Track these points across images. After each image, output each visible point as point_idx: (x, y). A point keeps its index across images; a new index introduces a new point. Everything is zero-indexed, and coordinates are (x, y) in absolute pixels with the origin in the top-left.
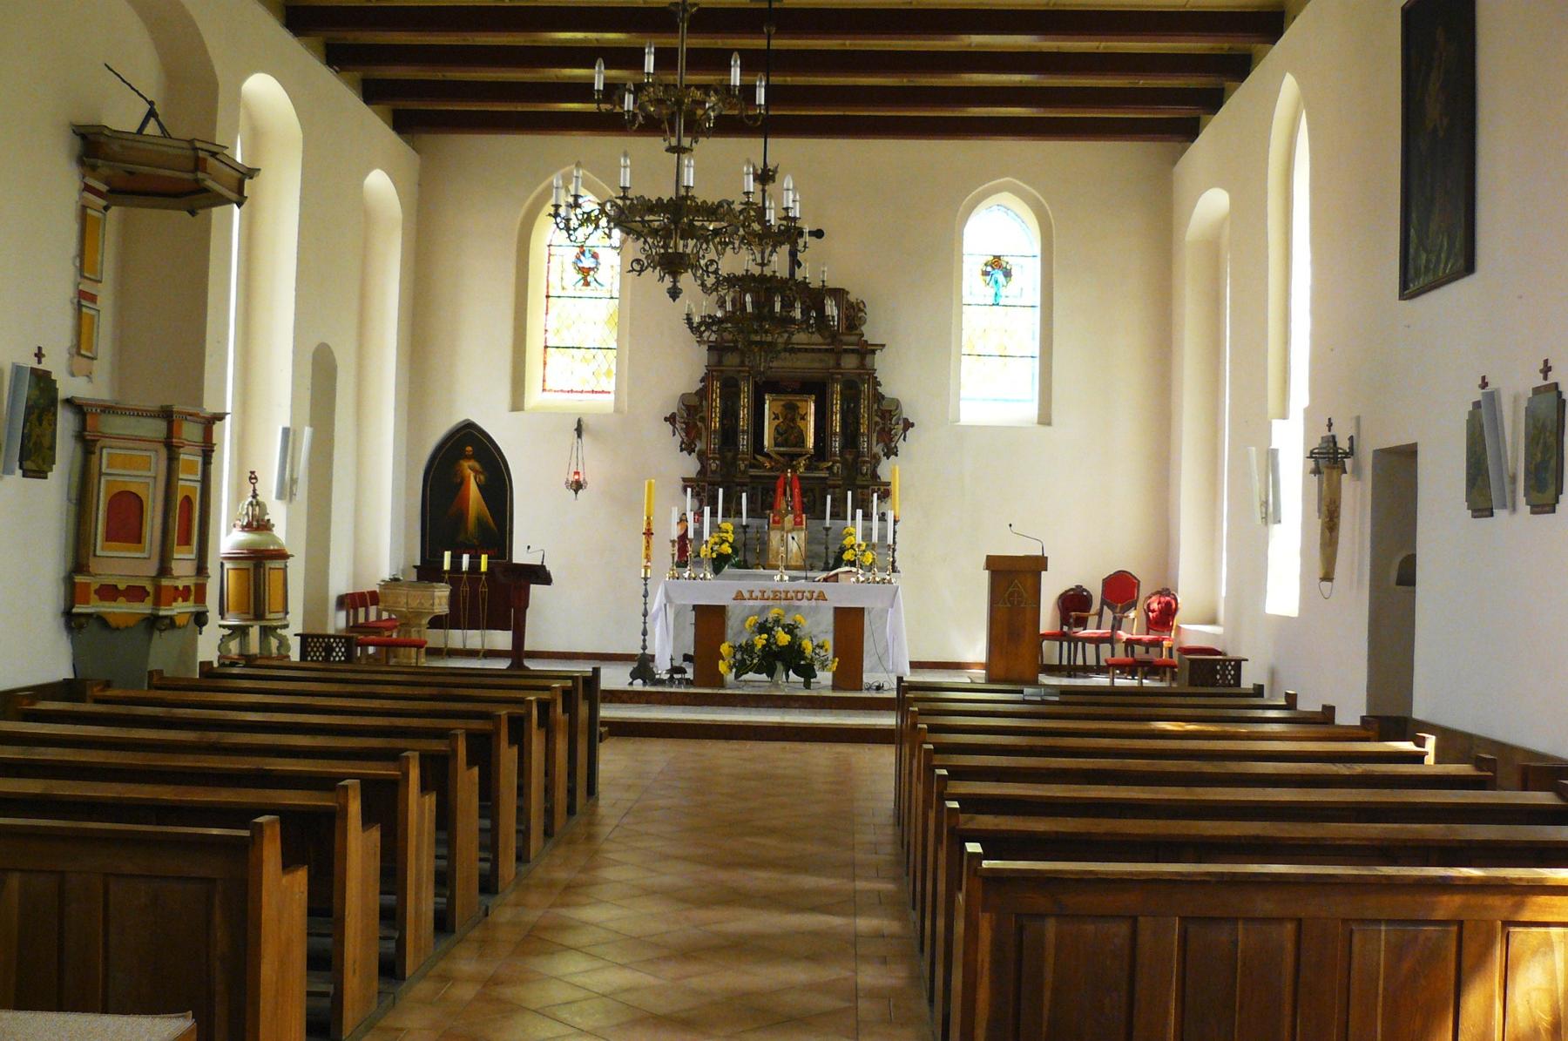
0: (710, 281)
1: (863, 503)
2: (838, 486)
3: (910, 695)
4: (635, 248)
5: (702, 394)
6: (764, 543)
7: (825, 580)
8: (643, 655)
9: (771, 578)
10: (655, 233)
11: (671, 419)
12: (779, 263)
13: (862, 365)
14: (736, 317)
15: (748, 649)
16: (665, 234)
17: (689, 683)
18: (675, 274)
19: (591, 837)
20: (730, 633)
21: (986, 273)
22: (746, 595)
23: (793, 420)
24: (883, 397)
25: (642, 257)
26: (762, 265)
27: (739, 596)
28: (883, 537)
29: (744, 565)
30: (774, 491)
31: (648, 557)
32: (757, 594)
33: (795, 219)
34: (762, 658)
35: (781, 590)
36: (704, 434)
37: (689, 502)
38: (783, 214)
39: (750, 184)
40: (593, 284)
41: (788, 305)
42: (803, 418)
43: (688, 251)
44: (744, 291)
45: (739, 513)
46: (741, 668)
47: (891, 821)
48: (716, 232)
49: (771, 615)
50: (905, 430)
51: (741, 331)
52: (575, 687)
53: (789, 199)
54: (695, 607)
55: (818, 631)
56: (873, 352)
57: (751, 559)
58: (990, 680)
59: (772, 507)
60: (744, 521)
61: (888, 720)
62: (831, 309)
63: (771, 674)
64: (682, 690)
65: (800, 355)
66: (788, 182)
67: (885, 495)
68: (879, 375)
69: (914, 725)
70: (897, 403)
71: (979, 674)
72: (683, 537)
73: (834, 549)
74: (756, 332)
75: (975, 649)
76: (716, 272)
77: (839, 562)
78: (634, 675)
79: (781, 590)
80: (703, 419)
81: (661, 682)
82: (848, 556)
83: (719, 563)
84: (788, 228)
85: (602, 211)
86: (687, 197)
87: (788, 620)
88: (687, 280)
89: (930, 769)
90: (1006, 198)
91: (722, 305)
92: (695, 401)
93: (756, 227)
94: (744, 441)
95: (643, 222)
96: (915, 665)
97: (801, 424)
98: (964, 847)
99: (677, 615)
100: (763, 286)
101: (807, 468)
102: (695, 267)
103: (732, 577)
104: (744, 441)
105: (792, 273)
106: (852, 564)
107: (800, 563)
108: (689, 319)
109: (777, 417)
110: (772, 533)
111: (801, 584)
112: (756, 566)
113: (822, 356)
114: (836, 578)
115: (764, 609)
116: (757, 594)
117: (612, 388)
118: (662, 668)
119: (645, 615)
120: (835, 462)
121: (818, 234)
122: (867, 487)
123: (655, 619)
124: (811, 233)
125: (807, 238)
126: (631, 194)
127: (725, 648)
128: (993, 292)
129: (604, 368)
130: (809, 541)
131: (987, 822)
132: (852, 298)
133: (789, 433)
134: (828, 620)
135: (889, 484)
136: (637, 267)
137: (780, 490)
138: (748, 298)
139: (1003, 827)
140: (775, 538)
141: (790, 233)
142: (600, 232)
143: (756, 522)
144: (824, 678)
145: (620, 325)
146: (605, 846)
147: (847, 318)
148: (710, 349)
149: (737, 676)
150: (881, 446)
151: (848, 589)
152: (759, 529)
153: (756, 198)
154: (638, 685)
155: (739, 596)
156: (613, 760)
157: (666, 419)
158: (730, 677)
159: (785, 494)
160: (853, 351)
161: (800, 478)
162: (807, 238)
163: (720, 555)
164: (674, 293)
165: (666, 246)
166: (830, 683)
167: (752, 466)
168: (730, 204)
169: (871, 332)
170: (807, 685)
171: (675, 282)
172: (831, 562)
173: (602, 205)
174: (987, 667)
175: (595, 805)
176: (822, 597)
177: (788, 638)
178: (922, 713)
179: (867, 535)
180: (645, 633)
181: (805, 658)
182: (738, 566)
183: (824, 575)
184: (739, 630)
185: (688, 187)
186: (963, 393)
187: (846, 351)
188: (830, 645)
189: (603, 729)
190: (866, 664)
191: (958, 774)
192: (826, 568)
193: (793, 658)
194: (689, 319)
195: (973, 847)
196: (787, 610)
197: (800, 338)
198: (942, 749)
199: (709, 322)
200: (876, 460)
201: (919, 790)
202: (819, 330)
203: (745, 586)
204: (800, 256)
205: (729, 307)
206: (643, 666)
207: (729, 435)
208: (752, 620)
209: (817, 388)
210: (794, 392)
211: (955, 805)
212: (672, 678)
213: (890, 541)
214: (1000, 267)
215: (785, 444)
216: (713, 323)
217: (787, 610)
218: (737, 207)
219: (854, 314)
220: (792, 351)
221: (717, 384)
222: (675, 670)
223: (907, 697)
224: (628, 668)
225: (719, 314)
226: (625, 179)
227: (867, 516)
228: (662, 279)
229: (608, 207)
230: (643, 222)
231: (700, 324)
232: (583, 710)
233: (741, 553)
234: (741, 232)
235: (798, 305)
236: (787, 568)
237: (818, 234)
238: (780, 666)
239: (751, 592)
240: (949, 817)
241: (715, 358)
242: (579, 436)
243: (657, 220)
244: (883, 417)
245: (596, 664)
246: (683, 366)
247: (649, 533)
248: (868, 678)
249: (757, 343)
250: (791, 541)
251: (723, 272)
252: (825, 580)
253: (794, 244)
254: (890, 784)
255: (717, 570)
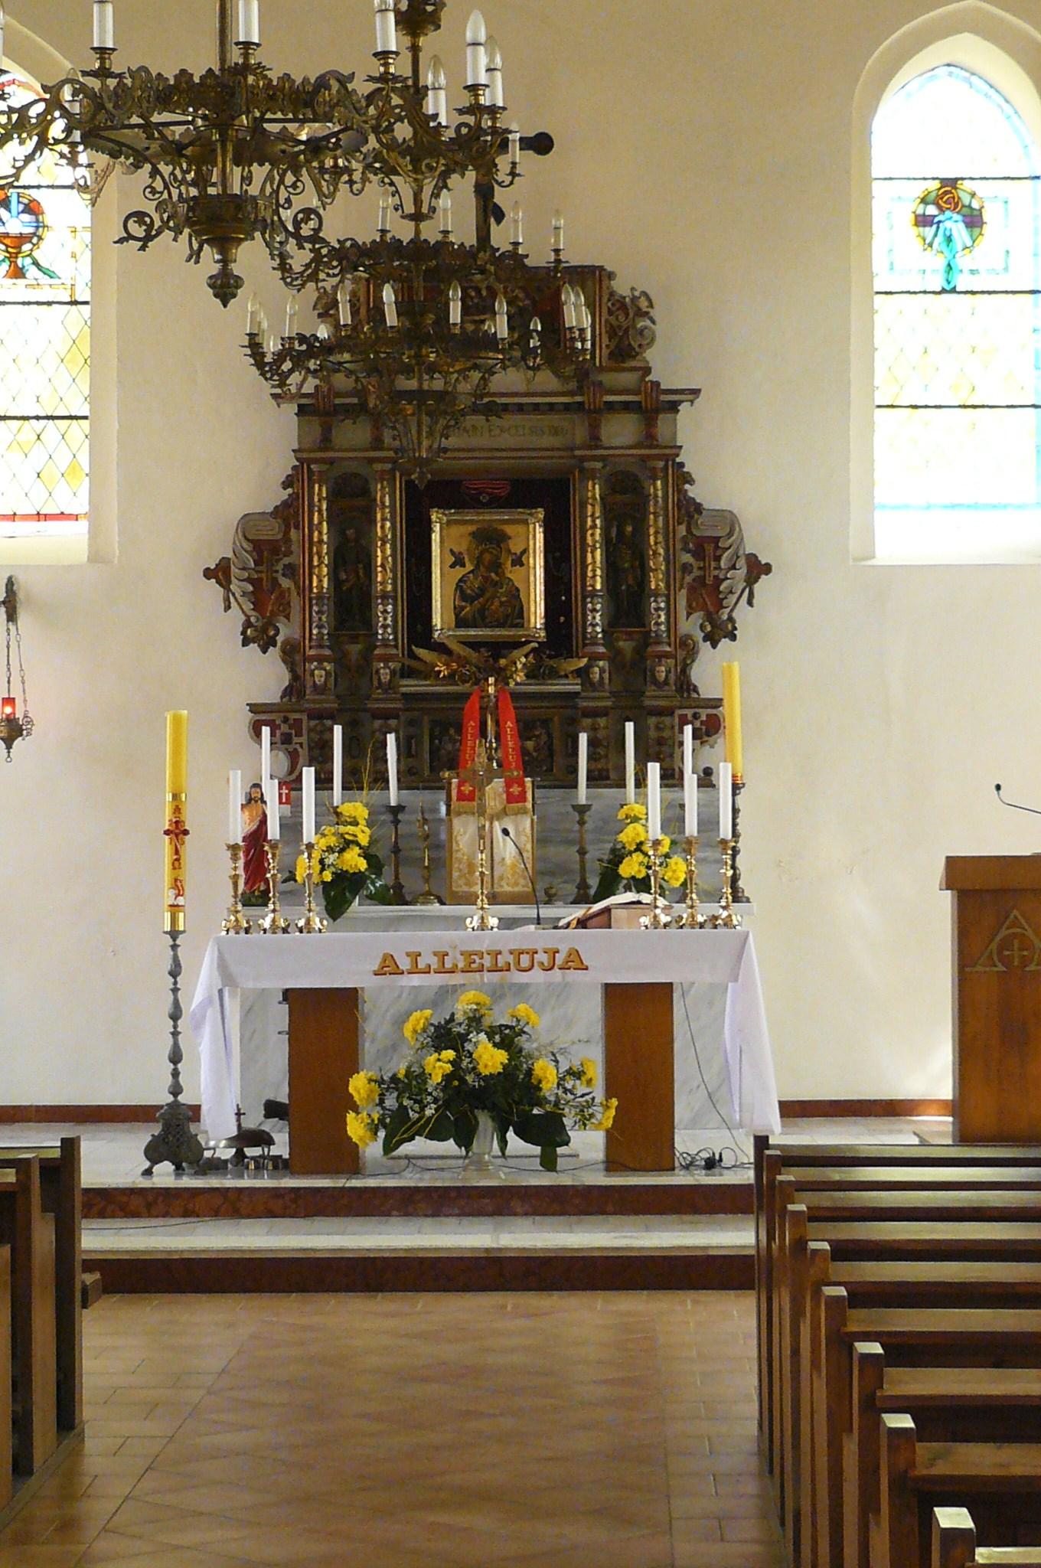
0: (299, 258)
1: (660, 749)
2: (603, 712)
3: (788, 1176)
4: (131, 188)
5: (288, 513)
6: (439, 851)
7: (582, 923)
8: (175, 1106)
9: (459, 922)
10: (175, 151)
11: (219, 573)
12: (453, 213)
13: (649, 438)
14: (361, 339)
15: (412, 1084)
16: (197, 154)
17: (280, 1165)
18: (224, 243)
19: (68, 1526)
20: (369, 1049)
21: (923, 221)
22: (404, 964)
23: (496, 566)
24: (698, 508)
25: (150, 208)
26: (417, 217)
27: (388, 967)
28: (709, 823)
29: (396, 896)
30: (460, 728)
31: (178, 886)
32: (427, 959)
33: (493, 110)
34: (444, 1106)
35: (483, 950)
36: (296, 602)
37: (267, 758)
38: (466, 100)
39: (390, 37)
40: (32, 272)
41: (478, 308)
42: (519, 561)
43: (254, 190)
44: (377, 280)
45: (381, 780)
46: (397, 1128)
47: (753, 1464)
48: (315, 146)
49: (462, 1006)
50: (752, 579)
51: (373, 369)
52: (23, 1185)
53: (478, 66)
54: (288, 995)
55: (569, 1039)
56: (673, 407)
57: (412, 881)
58: (964, 1137)
59: (453, 764)
60: (393, 796)
61: (737, 1236)
62: (576, 313)
63: (465, 1139)
64: (266, 1182)
65: (510, 420)
66: (476, 28)
67: (710, 728)
68: (689, 460)
69: (800, 1244)
70: (730, 521)
71: (939, 1127)
72: (256, 838)
73: (598, 852)
74: (408, 371)
75: (929, 1070)
76: (315, 238)
77: (610, 883)
78: (154, 1153)
79: (483, 950)
80: (291, 571)
81: (217, 1166)
82: (630, 868)
83: (339, 893)
84: (477, 131)
85: (54, 103)
86: (245, 69)
87: (500, 1017)
88: (252, 257)
89: (843, 1342)
90: (968, 47)
91: (327, 309)
92: (272, 531)
93: (403, 131)
94: (386, 618)
95: (147, 127)
96: (792, 1110)
97: (514, 574)
98: (929, 1519)
99: (247, 1013)
100: (420, 266)
101: (532, 674)
102: (264, 226)
103: (370, 924)
104: (386, 618)
105: (484, 236)
106: (642, 885)
107: (523, 886)
108: (255, 346)
109: (459, 562)
110: (457, 823)
111: (529, 935)
112: (424, 897)
113: (554, 419)
114: (605, 918)
115: (447, 993)
116: (427, 959)
117: (81, 505)
118: (216, 1134)
119: (175, 1016)
120: (594, 658)
121: (541, 144)
122: (670, 712)
123: (198, 1026)
124: (527, 143)
125: (516, 153)
126: (117, 65)
127: (359, 1085)
128: (940, 262)
129: (63, 459)
130: (541, 840)
131: (980, 1459)
132: (621, 287)
133: (488, 597)
134: (590, 1013)
135: (717, 703)
136: (138, 231)
137: (472, 725)
138: (388, 294)
139: (1018, 1471)
140: (464, 832)
141: (478, 146)
142: (48, 157)
143: (417, 798)
144: (587, 1145)
145: (95, 363)
146: (102, 1546)
147: (612, 332)
148: (302, 411)
149: (389, 1147)
150: (698, 617)
151: (633, 943)
152: (427, 816)
153: (400, 67)
154: (165, 1175)
155: (388, 967)
156: (114, 1347)
157: (208, 574)
158: (372, 1150)
159: (483, 733)
160: (626, 407)
161: (516, 696)
162: (516, 153)
163: (341, 876)
164: (225, 287)
165: (201, 182)
166: (600, 1155)
167: (407, 673)
168: (343, 80)
169: (667, 363)
170: (549, 1162)
171: (225, 262)
172: (594, 882)
173: (52, 91)
174: (956, 1108)
175: (77, 1453)
176: (575, 962)
177: (501, 1056)
178: (816, 1215)
179: (673, 818)
180: (176, 1057)
181: (540, 1102)
182: (382, 898)
183: (579, 912)
184: (391, 1040)
185: (247, 45)
186: (880, 495)
187: (611, 407)
188: (597, 1071)
189: (90, 1278)
190: (683, 1109)
191: (907, 1351)
192: (582, 897)
193: (514, 1102)
194: (255, 346)
195: (953, 1518)
196: (498, 993)
197: (508, 380)
198: (865, 1296)
199: (302, 351)
200: (687, 651)
201: (817, 1391)
202: (551, 362)
203: (400, 942)
204: (500, 197)
205: (345, 316)
206: (173, 1131)
207: (351, 604)
208: (419, 1019)
209: (548, 493)
210: (497, 503)
211: (906, 1422)
212: (240, 1155)
213: (725, 831)
214: (955, 204)
215: (480, 619)
216: (310, 353)
217: (498, 993)
218: (362, 87)
219: (626, 324)
220: (492, 410)
221: (320, 491)
222: (246, 1138)
223: (774, 1183)
224: (143, 1136)
225: (323, 332)
226: (104, 29)
227: (672, 778)
228: (195, 255)
229: (67, 93)
230: (147, 127)
231: (280, 357)
232: (43, 1236)
233: (388, 871)
234: (373, 142)
235: (502, 306)
236: (494, 899)
237: (541, 144)
238: (485, 1122)
239: (415, 956)
240: (893, 1449)
241: (317, 430)
242: (11, 617)
243: (179, 123)
244: (699, 553)
245: (68, 1130)
246: (243, 455)
247: (178, 831)
248: (687, 1142)
249: (409, 395)
250: (497, 836)
251: (332, 234)
252: (582, 923)
253: (487, 169)
254: (748, 1381)
255: (335, 908)
